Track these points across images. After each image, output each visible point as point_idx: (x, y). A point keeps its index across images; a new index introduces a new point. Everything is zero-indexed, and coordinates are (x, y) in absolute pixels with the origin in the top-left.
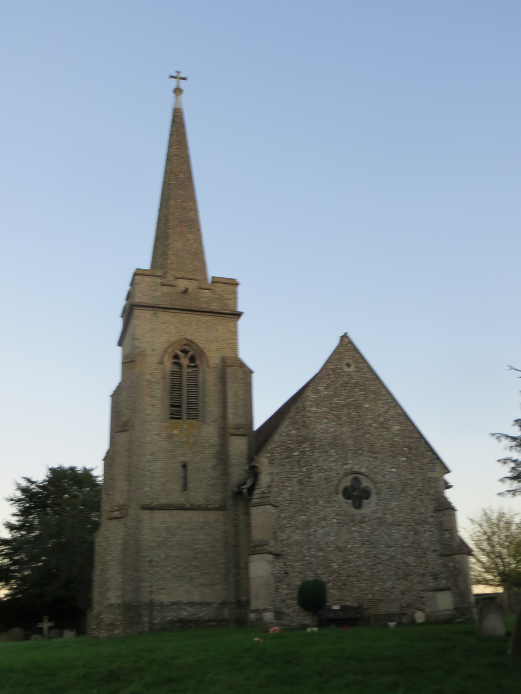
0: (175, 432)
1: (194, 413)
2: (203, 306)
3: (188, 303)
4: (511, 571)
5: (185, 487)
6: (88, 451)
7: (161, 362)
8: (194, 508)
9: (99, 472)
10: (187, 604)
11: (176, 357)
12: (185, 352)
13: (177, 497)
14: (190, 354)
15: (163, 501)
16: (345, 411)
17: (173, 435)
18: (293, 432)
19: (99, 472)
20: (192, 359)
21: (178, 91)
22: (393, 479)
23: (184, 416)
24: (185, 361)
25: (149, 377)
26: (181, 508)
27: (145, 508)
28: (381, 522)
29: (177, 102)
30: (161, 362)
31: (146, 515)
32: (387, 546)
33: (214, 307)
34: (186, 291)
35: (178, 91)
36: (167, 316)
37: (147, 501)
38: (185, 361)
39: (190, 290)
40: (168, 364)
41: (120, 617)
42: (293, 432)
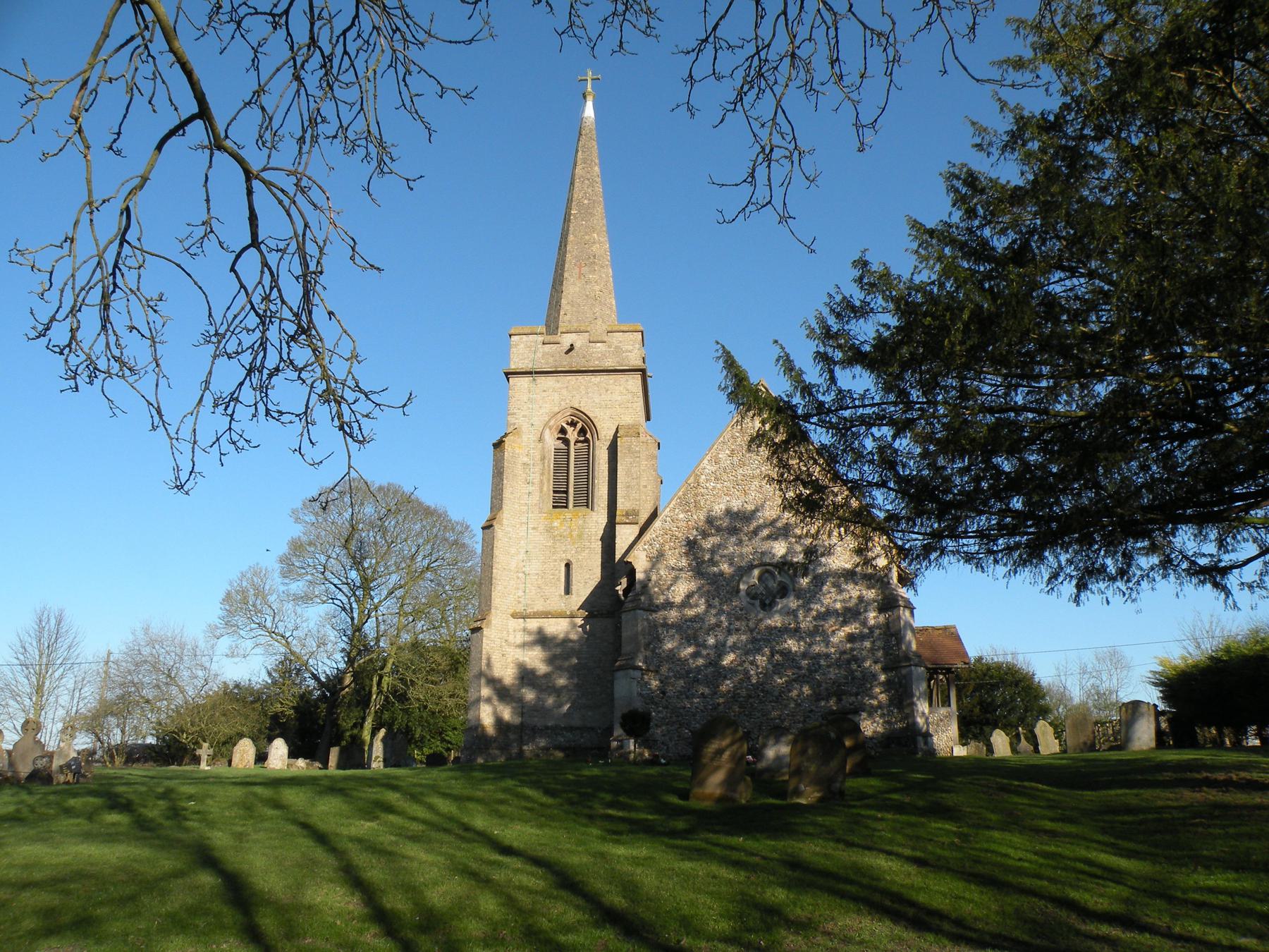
0: (556, 524)
2: (595, 364)
3: (575, 361)
4: (913, 704)
7: (541, 439)
10: (565, 728)
11: (563, 431)
12: (573, 424)
14: (579, 426)
17: (552, 528)
18: (681, 516)
20: (583, 432)
22: (445, 796)
24: (572, 435)
25: (525, 459)
30: (541, 439)
33: (609, 363)
34: (572, 348)
36: (549, 381)
38: (572, 435)
39: (577, 345)
40: (552, 442)
42: (681, 516)
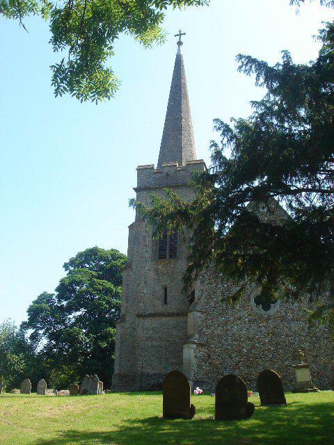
1: (173, 254)
5: (166, 303)
6: (116, 240)
8: (170, 315)
9: (123, 249)
13: (159, 307)
15: (151, 311)
16: (303, 193)
17: (158, 269)
19: (123, 249)
21: (180, 43)
23: (168, 257)
26: (162, 315)
27: (139, 316)
28: (283, 319)
29: (179, 50)
31: (141, 320)
32: (287, 336)
35: (180, 43)
37: (141, 312)
41: (328, 29)
